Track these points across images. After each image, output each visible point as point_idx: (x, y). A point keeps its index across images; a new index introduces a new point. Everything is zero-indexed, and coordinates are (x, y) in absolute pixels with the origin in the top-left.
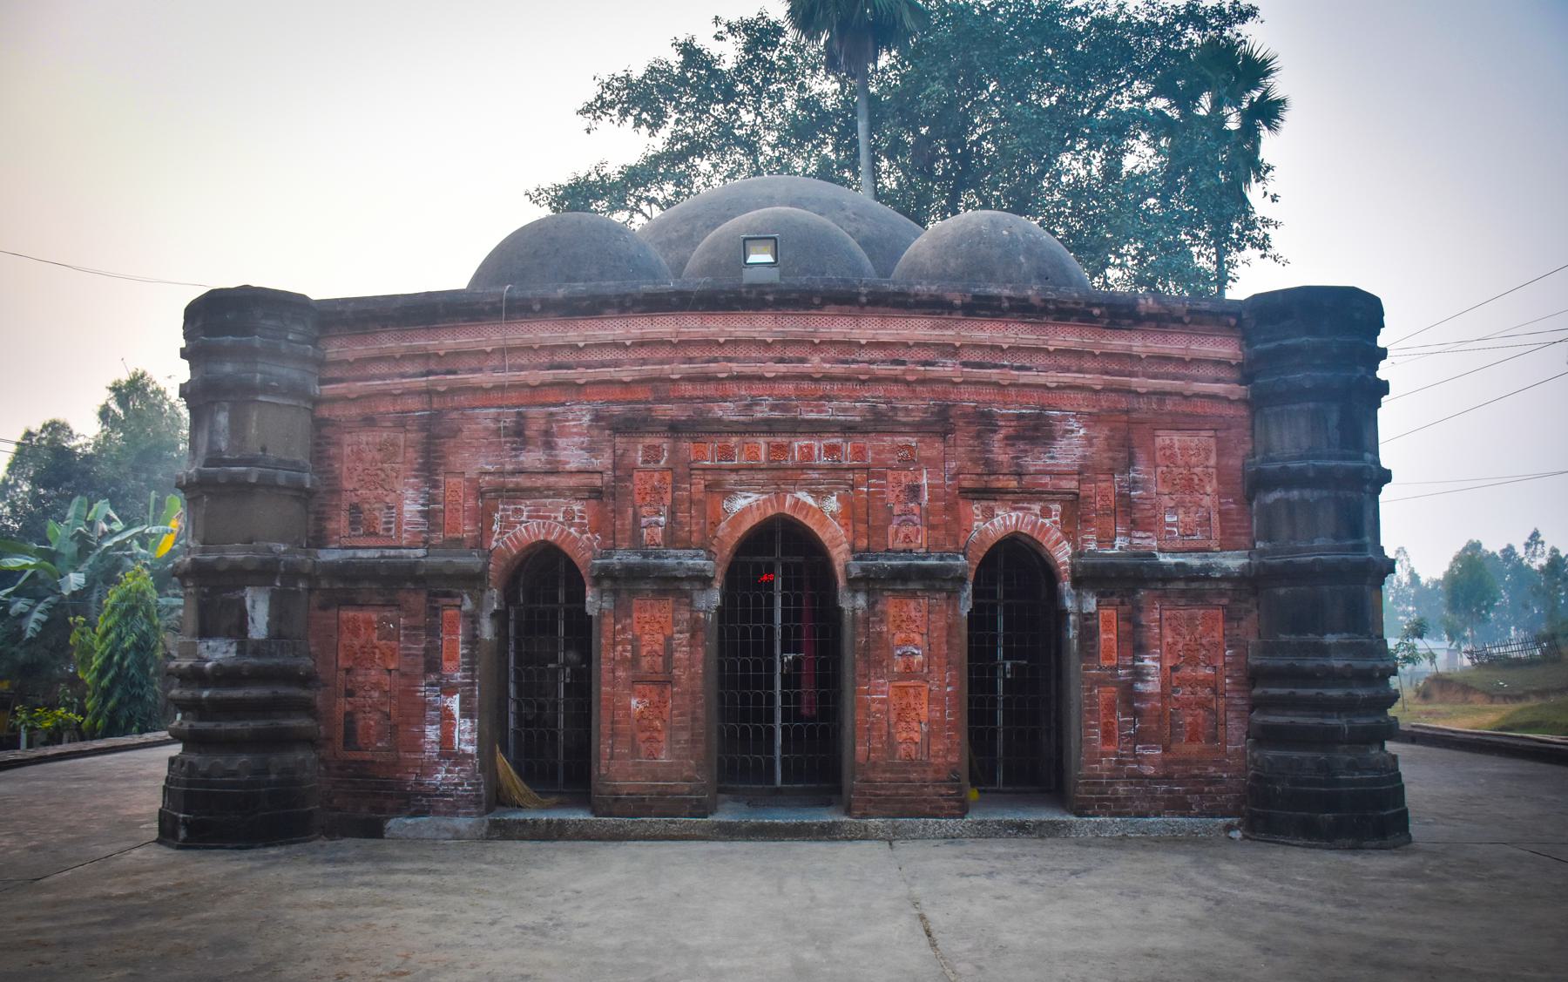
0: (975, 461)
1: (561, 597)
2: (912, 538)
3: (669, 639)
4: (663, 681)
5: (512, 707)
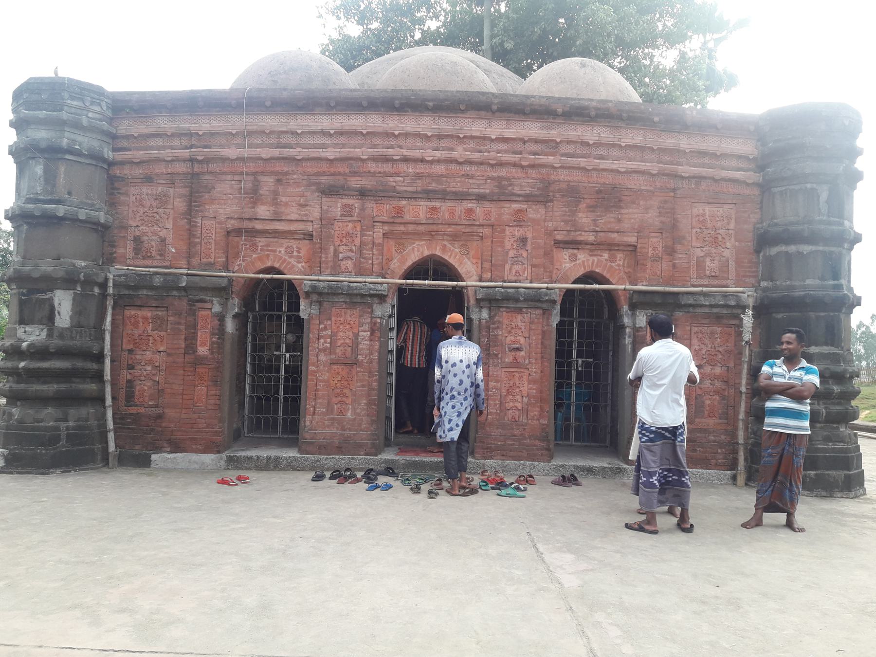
0: (566, 222)
1: (285, 308)
2: (521, 274)
3: (356, 335)
4: (351, 363)
5: (248, 380)
